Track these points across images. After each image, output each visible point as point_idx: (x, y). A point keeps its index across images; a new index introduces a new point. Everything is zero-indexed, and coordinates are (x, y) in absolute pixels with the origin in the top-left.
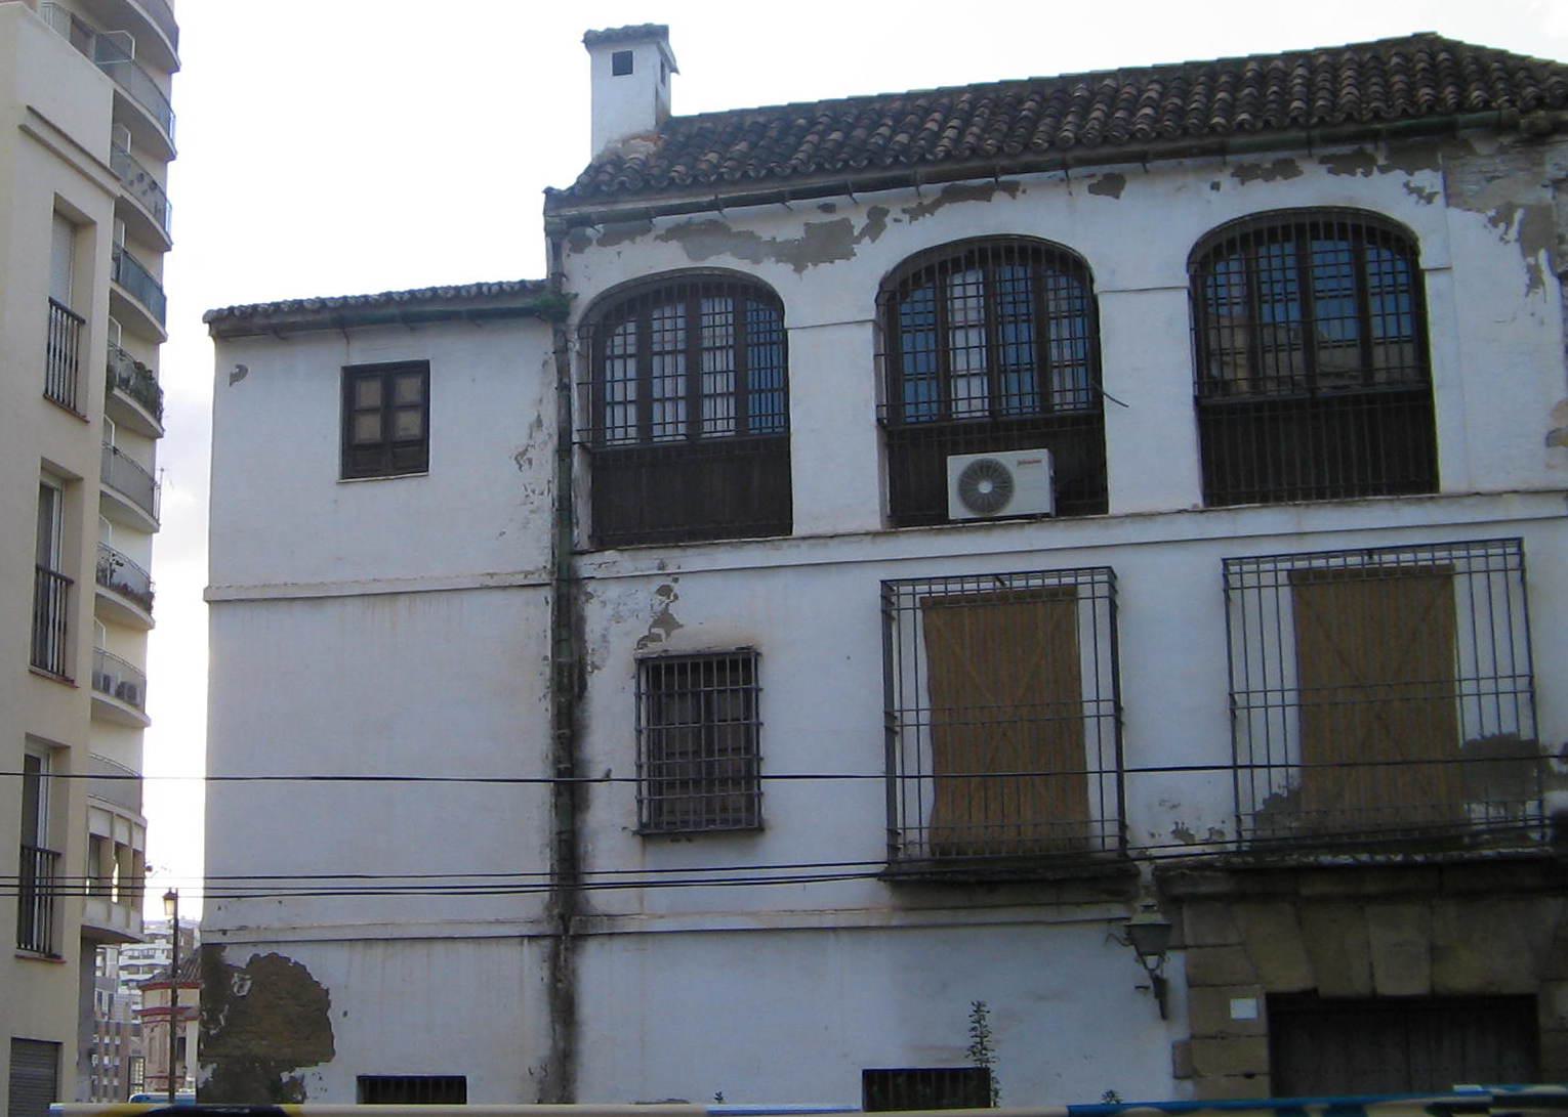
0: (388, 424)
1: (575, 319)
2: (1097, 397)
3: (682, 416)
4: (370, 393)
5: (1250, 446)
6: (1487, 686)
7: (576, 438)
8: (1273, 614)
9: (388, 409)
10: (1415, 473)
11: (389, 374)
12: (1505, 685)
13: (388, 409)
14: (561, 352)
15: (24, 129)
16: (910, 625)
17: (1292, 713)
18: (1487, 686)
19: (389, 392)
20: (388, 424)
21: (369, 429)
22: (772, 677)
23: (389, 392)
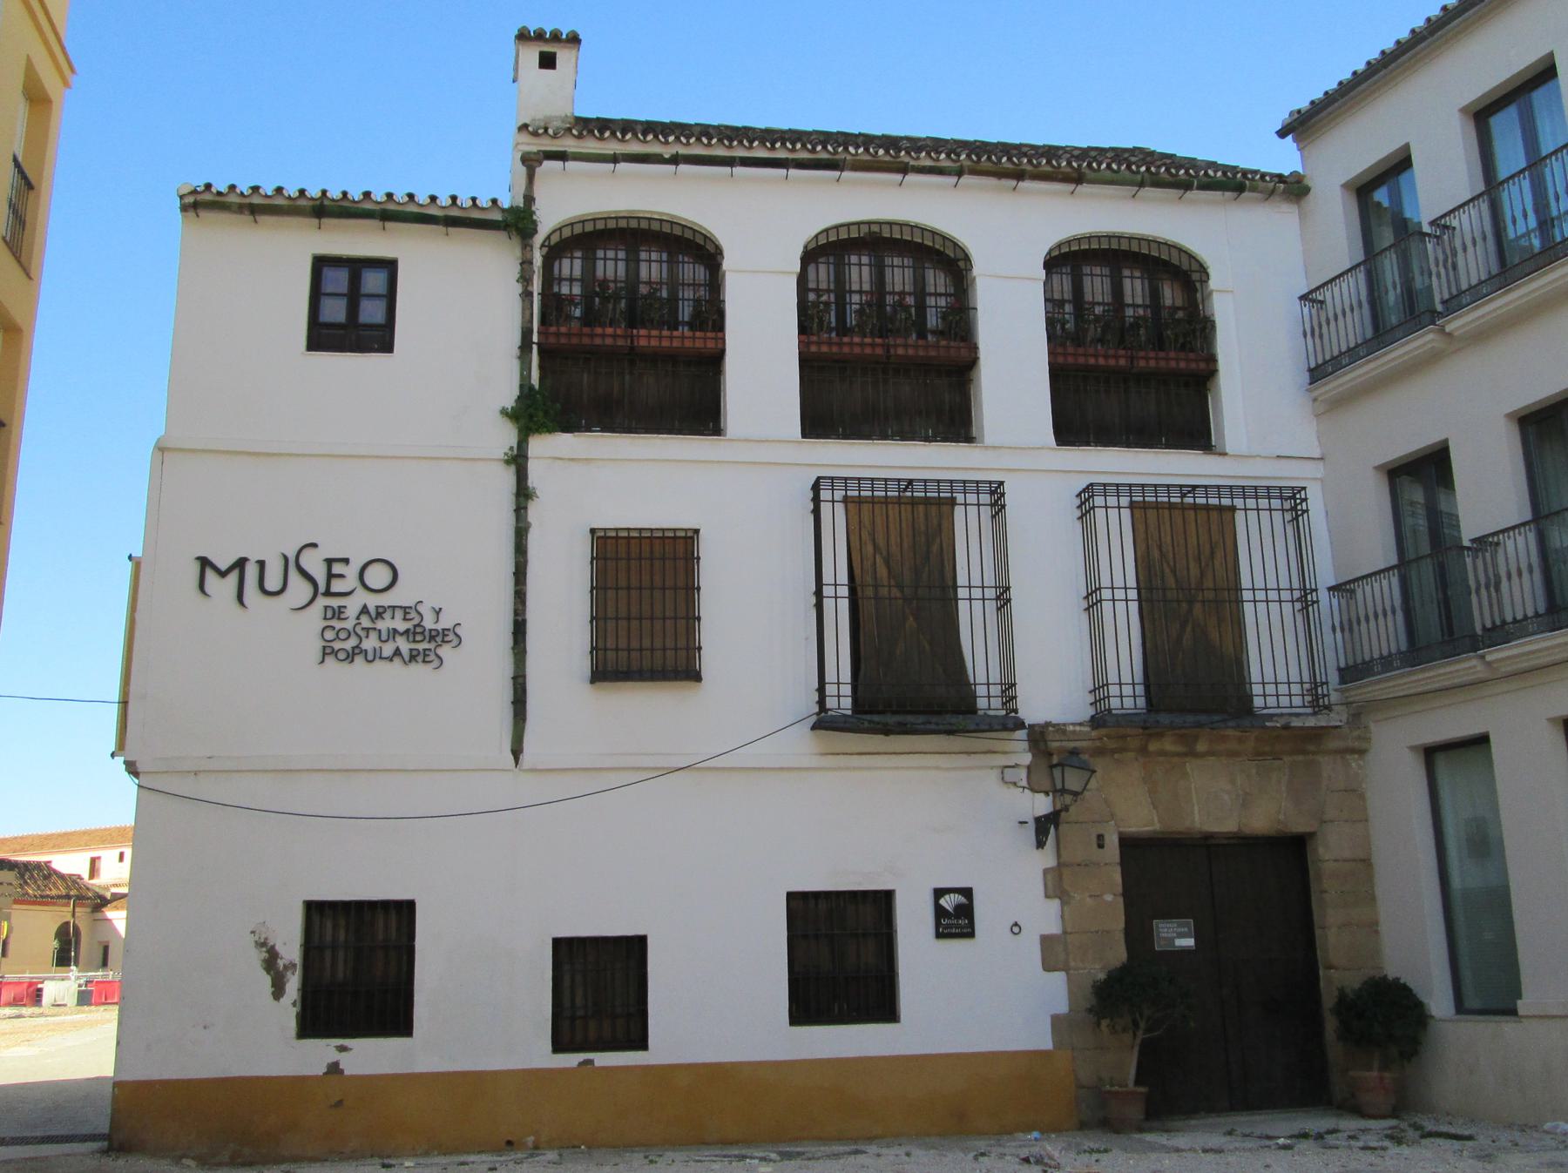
0: (353, 309)
1: (539, 239)
2: (297, 1159)
3: (600, 264)
4: (337, 280)
5: (1091, 401)
6: (977, 593)
7: (535, 339)
8: (1116, 526)
9: (354, 297)
10: (1194, 431)
11: (357, 266)
12: (1285, 595)
13: (354, 297)
14: (526, 263)
15: (73, 70)
16: (836, 520)
17: (1134, 606)
18: (977, 593)
19: (355, 281)
20: (353, 309)
21: (335, 311)
22: (708, 552)
23: (355, 281)
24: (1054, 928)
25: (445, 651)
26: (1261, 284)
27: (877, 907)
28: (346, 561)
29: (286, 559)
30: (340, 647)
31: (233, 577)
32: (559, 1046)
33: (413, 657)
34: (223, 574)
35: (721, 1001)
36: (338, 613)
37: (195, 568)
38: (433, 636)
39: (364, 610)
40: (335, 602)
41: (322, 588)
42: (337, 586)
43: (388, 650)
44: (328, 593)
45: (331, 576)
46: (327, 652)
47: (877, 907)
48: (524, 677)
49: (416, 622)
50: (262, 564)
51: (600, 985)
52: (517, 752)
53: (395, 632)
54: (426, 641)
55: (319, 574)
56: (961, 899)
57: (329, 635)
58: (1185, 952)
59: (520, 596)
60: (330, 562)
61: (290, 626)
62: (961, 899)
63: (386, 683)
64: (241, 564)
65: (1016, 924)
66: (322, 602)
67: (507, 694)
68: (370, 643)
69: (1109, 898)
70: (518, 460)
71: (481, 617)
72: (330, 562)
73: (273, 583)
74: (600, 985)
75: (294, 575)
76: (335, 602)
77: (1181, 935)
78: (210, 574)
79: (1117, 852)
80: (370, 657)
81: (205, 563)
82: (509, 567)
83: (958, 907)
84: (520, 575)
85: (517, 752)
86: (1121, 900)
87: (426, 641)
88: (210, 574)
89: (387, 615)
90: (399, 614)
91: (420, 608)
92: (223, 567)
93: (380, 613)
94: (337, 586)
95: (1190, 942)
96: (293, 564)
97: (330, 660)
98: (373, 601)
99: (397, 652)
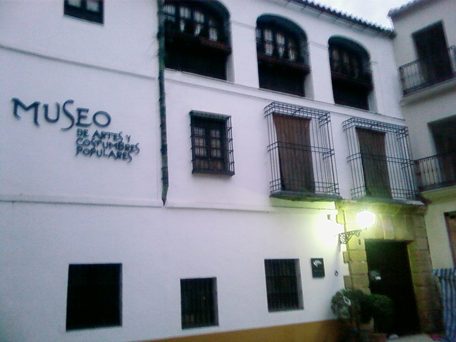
24: (347, 273)
25: (132, 155)
26: (387, 66)
27: (291, 265)
28: (87, 111)
29: (58, 106)
30: (86, 148)
31: (32, 112)
32: (185, 325)
33: (119, 156)
34: (27, 109)
35: (243, 304)
36: (85, 133)
37: (12, 105)
38: (127, 148)
39: (96, 134)
40: (83, 129)
41: (76, 121)
42: (83, 121)
43: (108, 152)
44: (78, 124)
45: (80, 117)
46: (79, 150)
47: (291, 265)
48: (167, 168)
49: (119, 141)
50: (46, 107)
51: (199, 299)
52: (164, 200)
53: (110, 145)
54: (124, 151)
55: (75, 115)
56: (320, 263)
57: (80, 143)
58: (379, 281)
59: (163, 134)
60: (80, 111)
61: (60, 139)
62: (320, 263)
63: (105, 169)
64: (35, 105)
65: (337, 272)
66: (75, 128)
67: (160, 176)
68: (99, 148)
69: (363, 262)
70: (161, 78)
71: (147, 140)
72: (80, 111)
73: (52, 115)
74: (199, 299)
75: (62, 115)
76: (83, 129)
77: (377, 275)
78: (20, 110)
79: (364, 246)
80: (99, 154)
81: (17, 103)
82: (158, 124)
83: (319, 265)
84: (163, 126)
85: (164, 200)
86: (366, 263)
87: (124, 151)
88: (20, 110)
89: (107, 136)
90: (112, 138)
91: (122, 135)
92: (27, 104)
93: (103, 136)
94: (83, 121)
95: (379, 278)
96: (62, 109)
97: (80, 155)
98: (100, 131)
99: (112, 154)
